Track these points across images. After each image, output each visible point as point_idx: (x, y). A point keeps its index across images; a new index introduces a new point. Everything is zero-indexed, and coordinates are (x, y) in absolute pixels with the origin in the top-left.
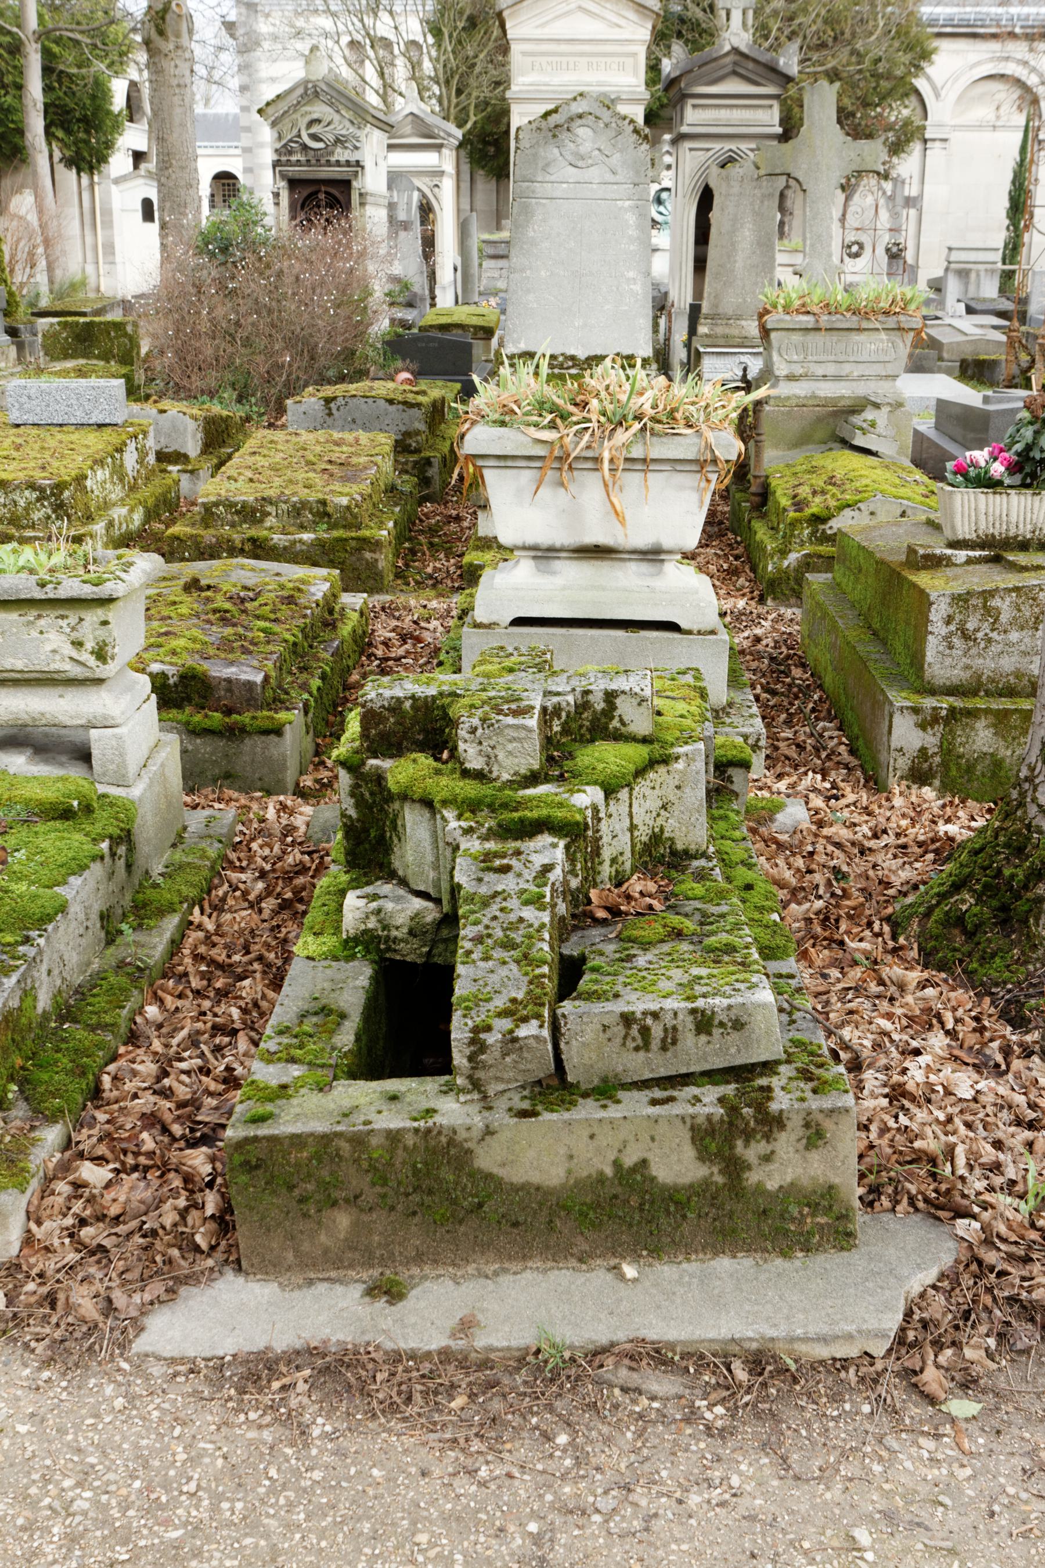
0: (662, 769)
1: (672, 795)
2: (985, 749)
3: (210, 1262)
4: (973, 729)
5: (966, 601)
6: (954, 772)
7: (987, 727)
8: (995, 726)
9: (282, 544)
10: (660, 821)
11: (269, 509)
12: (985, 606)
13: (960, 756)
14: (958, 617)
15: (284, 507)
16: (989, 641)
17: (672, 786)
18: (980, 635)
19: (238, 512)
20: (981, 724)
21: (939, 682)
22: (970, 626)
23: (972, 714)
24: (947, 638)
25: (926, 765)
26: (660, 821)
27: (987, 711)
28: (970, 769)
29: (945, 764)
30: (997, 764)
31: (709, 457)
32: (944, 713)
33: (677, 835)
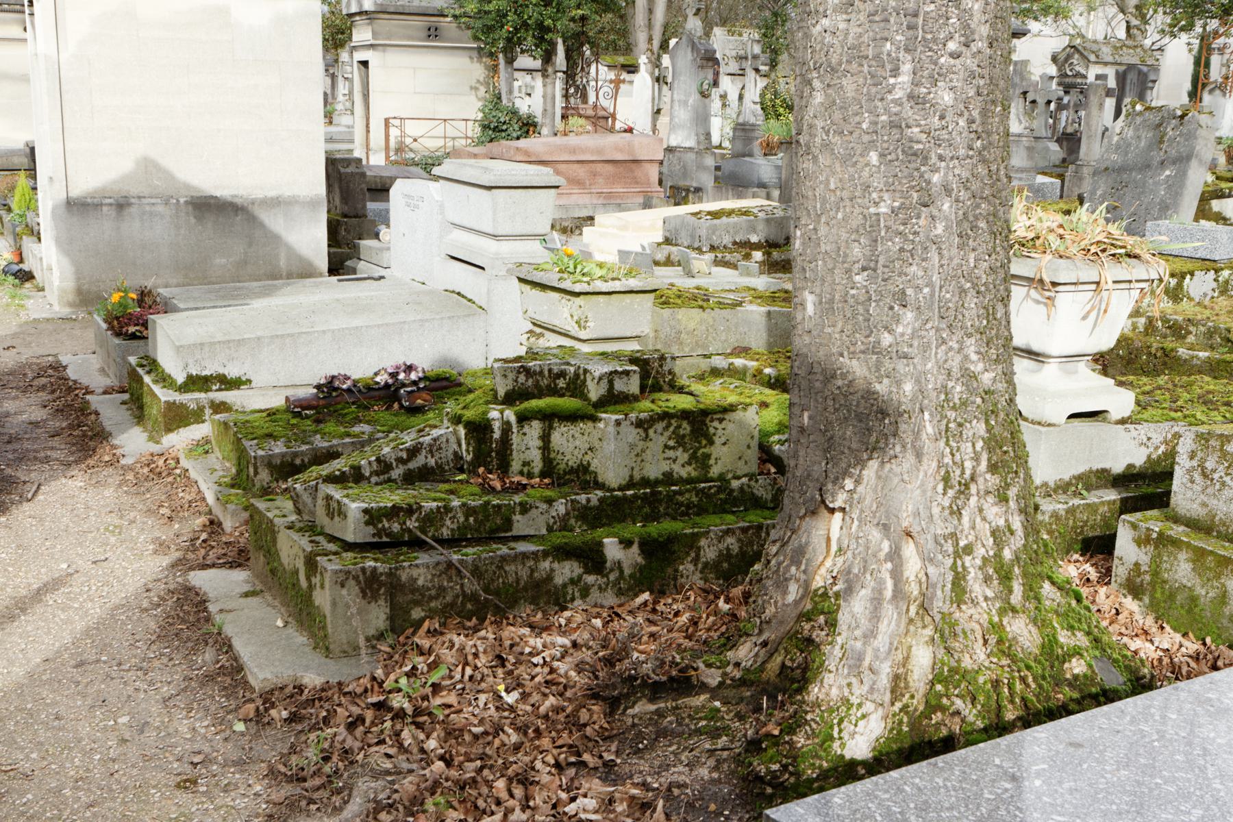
0: (590, 424)
1: (597, 444)
2: (1184, 581)
3: (186, 514)
4: (1176, 558)
5: (1207, 441)
6: (1158, 595)
7: (1187, 560)
8: (1194, 562)
9: (1184, 356)
10: (587, 458)
11: (1191, 328)
12: (1221, 450)
13: (1165, 582)
14: (1200, 454)
15: (1202, 329)
16: (1223, 484)
17: (596, 438)
18: (1216, 476)
19: (1169, 327)
20: (1183, 556)
21: (1181, 511)
22: (1209, 465)
23: (1176, 543)
24: (1189, 471)
25: (1138, 580)
26: (587, 458)
27: (1188, 545)
28: (1172, 596)
29: (1153, 584)
30: (1193, 599)
31: (1038, 277)
32: (1155, 535)
33: (598, 471)
